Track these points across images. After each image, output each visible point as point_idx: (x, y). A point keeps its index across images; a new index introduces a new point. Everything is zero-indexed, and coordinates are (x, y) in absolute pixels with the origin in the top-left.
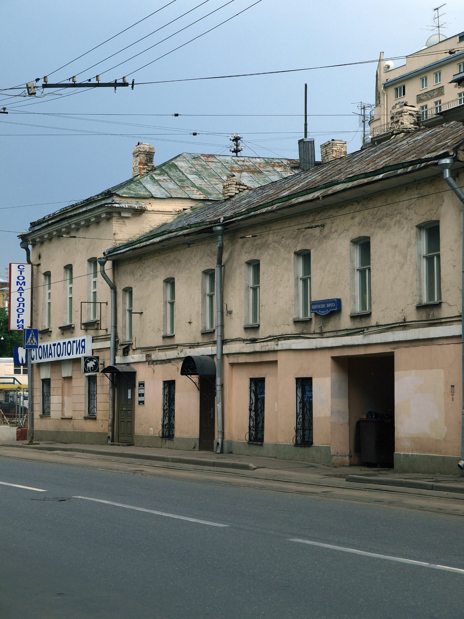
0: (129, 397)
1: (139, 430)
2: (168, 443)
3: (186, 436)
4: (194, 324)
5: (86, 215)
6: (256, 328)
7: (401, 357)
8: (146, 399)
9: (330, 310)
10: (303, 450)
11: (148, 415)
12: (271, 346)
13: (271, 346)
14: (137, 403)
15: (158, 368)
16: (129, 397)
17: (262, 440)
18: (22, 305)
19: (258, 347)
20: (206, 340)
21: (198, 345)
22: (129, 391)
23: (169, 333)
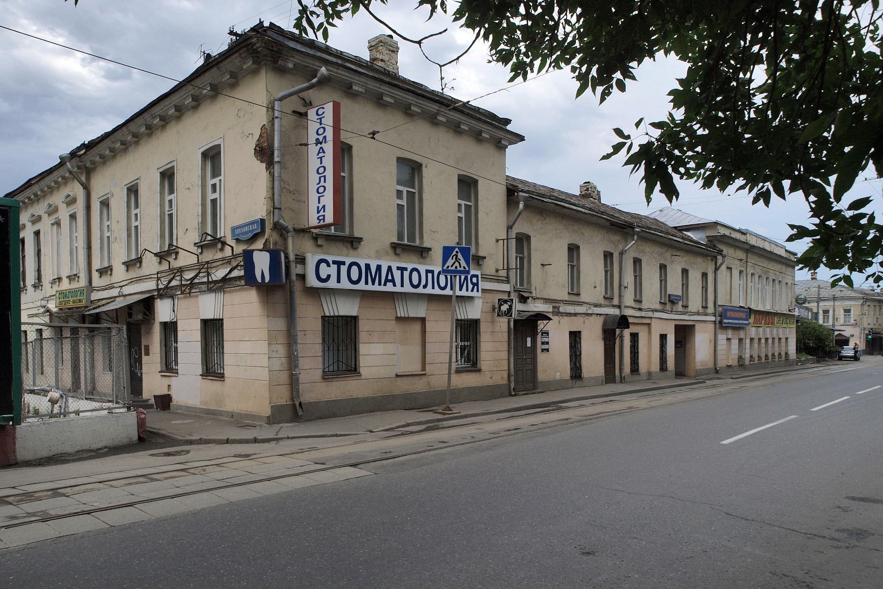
0: (529, 345)
1: (542, 376)
2: (579, 383)
3: (592, 375)
4: (598, 288)
5: (306, 60)
6: (640, 302)
7: (698, 327)
8: (550, 346)
9: (672, 300)
10: (663, 373)
11: (554, 360)
12: (650, 314)
13: (650, 314)
14: (539, 351)
15: (566, 319)
16: (529, 345)
17: (638, 370)
18: (322, 179)
19: (643, 314)
20: (607, 303)
21: (600, 306)
22: (529, 340)
23: (608, 296)
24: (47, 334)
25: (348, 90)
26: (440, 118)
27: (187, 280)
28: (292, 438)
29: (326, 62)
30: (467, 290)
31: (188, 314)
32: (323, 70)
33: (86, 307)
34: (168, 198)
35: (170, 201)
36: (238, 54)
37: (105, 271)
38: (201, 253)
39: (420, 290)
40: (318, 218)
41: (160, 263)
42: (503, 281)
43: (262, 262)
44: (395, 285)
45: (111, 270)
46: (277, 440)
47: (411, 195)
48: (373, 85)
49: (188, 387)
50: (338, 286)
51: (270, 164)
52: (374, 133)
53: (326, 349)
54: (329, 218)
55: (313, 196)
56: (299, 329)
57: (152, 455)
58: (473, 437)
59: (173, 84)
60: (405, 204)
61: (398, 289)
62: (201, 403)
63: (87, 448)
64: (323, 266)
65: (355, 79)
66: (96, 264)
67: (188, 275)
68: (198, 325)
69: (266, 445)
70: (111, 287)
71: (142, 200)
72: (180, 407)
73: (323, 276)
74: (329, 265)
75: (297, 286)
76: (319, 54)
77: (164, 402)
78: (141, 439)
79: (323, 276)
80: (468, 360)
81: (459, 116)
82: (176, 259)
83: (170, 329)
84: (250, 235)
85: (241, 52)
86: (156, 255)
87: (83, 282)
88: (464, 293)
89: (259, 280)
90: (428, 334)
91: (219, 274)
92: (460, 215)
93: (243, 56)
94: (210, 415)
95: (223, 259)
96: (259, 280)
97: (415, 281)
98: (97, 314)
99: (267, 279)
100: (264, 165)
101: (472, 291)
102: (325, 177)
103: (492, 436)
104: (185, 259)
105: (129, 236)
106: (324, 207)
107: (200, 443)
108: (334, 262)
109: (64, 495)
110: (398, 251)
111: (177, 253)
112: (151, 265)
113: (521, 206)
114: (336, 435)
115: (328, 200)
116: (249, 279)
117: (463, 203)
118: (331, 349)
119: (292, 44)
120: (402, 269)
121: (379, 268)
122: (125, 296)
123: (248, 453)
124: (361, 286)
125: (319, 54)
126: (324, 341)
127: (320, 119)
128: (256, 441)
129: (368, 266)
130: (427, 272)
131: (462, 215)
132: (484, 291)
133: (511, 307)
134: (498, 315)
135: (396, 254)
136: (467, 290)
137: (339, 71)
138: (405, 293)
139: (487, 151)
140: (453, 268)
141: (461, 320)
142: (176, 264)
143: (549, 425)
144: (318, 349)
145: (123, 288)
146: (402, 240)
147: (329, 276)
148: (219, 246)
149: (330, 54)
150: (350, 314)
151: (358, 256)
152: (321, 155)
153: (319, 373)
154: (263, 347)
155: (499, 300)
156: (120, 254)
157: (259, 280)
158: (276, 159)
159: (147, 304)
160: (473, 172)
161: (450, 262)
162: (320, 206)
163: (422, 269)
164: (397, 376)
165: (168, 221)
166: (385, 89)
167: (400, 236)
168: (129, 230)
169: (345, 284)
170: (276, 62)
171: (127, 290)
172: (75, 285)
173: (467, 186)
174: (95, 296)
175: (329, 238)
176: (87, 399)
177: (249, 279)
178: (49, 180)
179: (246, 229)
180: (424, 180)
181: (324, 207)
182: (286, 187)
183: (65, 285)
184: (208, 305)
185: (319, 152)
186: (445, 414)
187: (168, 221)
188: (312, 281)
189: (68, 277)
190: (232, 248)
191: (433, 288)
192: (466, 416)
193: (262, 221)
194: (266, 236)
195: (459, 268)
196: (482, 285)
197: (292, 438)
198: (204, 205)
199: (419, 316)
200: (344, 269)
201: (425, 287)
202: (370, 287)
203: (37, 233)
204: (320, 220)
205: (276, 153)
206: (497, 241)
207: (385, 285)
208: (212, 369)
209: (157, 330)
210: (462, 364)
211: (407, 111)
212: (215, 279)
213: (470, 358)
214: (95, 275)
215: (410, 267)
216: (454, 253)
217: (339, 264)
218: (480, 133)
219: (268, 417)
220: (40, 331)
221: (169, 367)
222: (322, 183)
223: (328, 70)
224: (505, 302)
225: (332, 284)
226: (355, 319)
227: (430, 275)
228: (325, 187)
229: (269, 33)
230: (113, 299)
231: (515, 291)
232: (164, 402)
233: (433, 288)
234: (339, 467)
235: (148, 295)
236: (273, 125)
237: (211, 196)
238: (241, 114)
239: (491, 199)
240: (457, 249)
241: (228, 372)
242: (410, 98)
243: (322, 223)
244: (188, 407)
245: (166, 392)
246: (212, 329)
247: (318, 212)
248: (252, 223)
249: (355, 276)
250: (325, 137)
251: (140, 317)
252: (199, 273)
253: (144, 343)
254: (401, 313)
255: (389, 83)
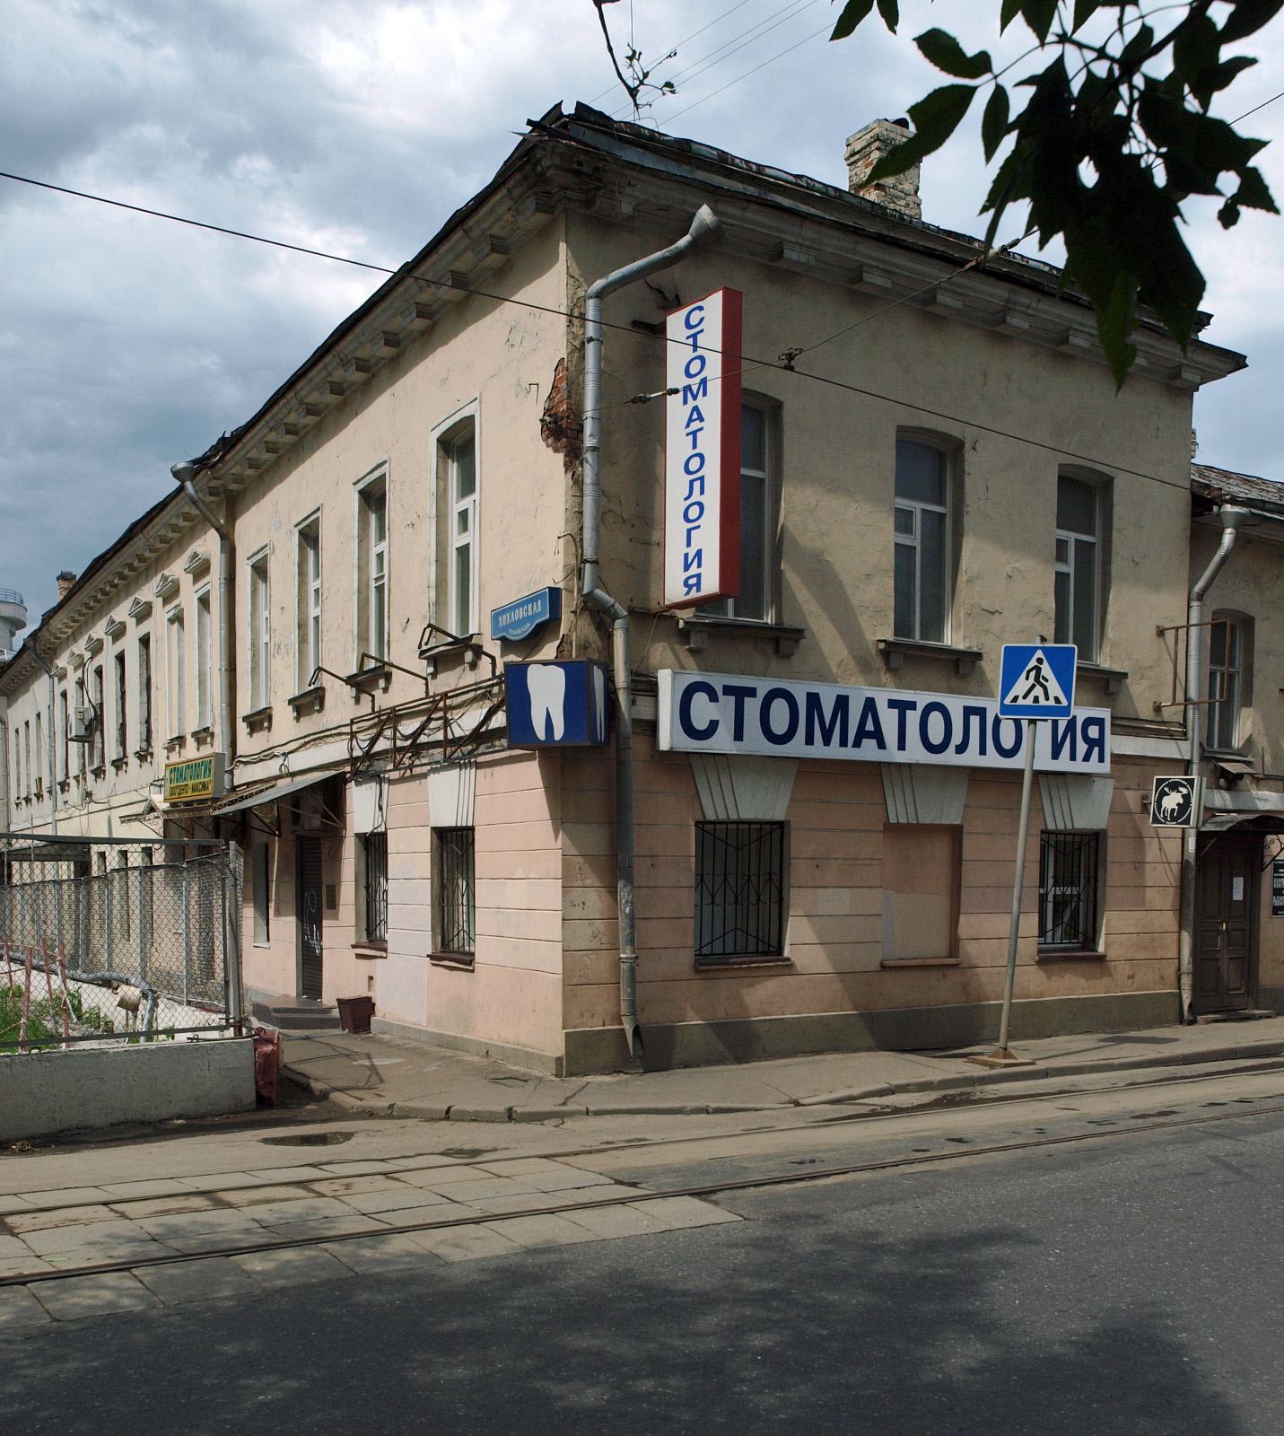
0: (1238, 895)
14: (1265, 912)
16: (1238, 895)
18: (697, 485)
22: (1238, 884)
24: (159, 858)
25: (773, 265)
26: (1014, 321)
27: (406, 738)
28: (599, 1113)
29: (714, 195)
30: (1073, 757)
31: (402, 814)
32: (705, 214)
33: (215, 800)
34: (374, 551)
35: (380, 556)
36: (504, 191)
37: (260, 720)
38: (434, 675)
39: (949, 757)
40: (686, 583)
41: (357, 700)
42: (1170, 736)
43: (547, 691)
44: (882, 745)
45: (270, 718)
46: (562, 1116)
47: (1084, 549)
48: (834, 243)
49: (405, 986)
50: (901, 757)
51: (573, 456)
52: (790, 357)
53: (707, 900)
54: (711, 583)
55: (674, 529)
56: (636, 851)
57: (266, 1141)
58: (1041, 1131)
59: (381, 279)
60: (917, 544)
61: (893, 754)
62: (429, 1022)
63: (139, 1117)
64: (700, 699)
65: (790, 231)
66: (244, 708)
67: (408, 727)
68: (424, 841)
69: (534, 1128)
70: (267, 755)
71: (326, 556)
72: (388, 1027)
73: (700, 723)
74: (713, 697)
75: (638, 745)
76: (700, 175)
77: (358, 1013)
78: (263, 1102)
79: (700, 723)
80: (1072, 932)
81: (769, 221)
82: (386, 690)
83: (374, 846)
84: (528, 628)
85: (511, 183)
86: (349, 681)
87: (219, 745)
88: (1063, 764)
89: (541, 733)
90: (966, 867)
91: (467, 721)
92: (1063, 568)
93: (516, 193)
94: (443, 1050)
95: (476, 686)
96: (541, 735)
97: (936, 736)
98: (244, 812)
99: (559, 733)
100: (560, 457)
101: (1087, 758)
102: (702, 479)
103: (1093, 1129)
104: (404, 690)
105: (303, 640)
106: (699, 553)
107: (390, 1117)
108: (728, 690)
109: (230, 1205)
110: (894, 661)
111: (388, 677)
112: (341, 705)
113: (1228, 537)
114: (706, 1111)
115: (709, 537)
116: (519, 732)
117: (1071, 536)
118: (719, 900)
119: (632, 155)
120: (903, 707)
121: (842, 703)
122: (293, 775)
123: (477, 1146)
124: (797, 747)
125: (700, 175)
126: (701, 877)
127: (694, 336)
128: (510, 1116)
129: (813, 700)
130: (968, 711)
131: (1069, 568)
132: (1118, 759)
133: (1187, 798)
134: (1156, 820)
135: (890, 669)
136: (1073, 757)
137: (749, 215)
138: (910, 765)
139: (1141, 400)
140: (1029, 701)
141: (1057, 833)
142: (385, 701)
143: (1257, 1105)
144: (686, 900)
145: (288, 756)
146: (910, 634)
147: (714, 725)
148: (469, 656)
149: (730, 174)
150: (768, 817)
151: (792, 675)
152: (695, 426)
153: (686, 958)
154: (552, 893)
155: (1160, 782)
156: (286, 683)
157: (541, 733)
158: (589, 442)
159: (330, 793)
160: (1099, 457)
161: (1021, 686)
162: (691, 555)
163: (955, 704)
164: (884, 967)
165: (374, 599)
166: (868, 252)
167: (902, 626)
168: (302, 626)
169: (756, 742)
170: (588, 203)
171: (298, 761)
172: (206, 750)
173: (1084, 496)
174: (243, 775)
175: (721, 632)
176: (189, 1003)
177: (519, 732)
178: (158, 527)
179: (520, 614)
180: (969, 483)
181: (699, 553)
182: (623, 511)
183: (191, 751)
184: (445, 796)
185: (690, 420)
186: (992, 1066)
187: (374, 599)
188: (668, 736)
189: (195, 734)
190: (493, 659)
191: (983, 751)
192: (1046, 1074)
193: (554, 593)
194: (563, 630)
195: (1043, 702)
196: (1118, 744)
197: (599, 1113)
198: (441, 562)
199: (945, 821)
200: (752, 707)
201: (961, 749)
202: (818, 751)
203: (145, 641)
204: (690, 587)
205: (589, 427)
206: (1161, 633)
207: (857, 744)
208: (452, 949)
209: (350, 850)
210: (1056, 938)
211: (927, 309)
212: (458, 733)
213: (1072, 927)
214: (242, 728)
215: (923, 699)
216: (1033, 663)
217: (741, 694)
218: (856, 274)
219: (558, 1060)
220: (148, 853)
221: (372, 939)
222: (696, 497)
223: (715, 212)
224: (1174, 786)
225: (722, 742)
226: (781, 826)
227: (974, 720)
228: (701, 505)
229: (575, 130)
230: (270, 781)
231: (1203, 758)
232: (358, 1013)
233: (983, 751)
234: (665, 1195)
235: (333, 773)
236: (582, 358)
237: (456, 540)
238: (516, 339)
239: (1146, 519)
240: (1039, 654)
241: (482, 950)
242: (935, 273)
243: (694, 594)
244: (404, 1028)
245: (363, 993)
246: (454, 848)
247: (687, 567)
248: (532, 599)
249: (779, 723)
250: (704, 382)
251: (317, 822)
252: (429, 720)
253: (325, 881)
254: (899, 812)
255: (879, 238)
